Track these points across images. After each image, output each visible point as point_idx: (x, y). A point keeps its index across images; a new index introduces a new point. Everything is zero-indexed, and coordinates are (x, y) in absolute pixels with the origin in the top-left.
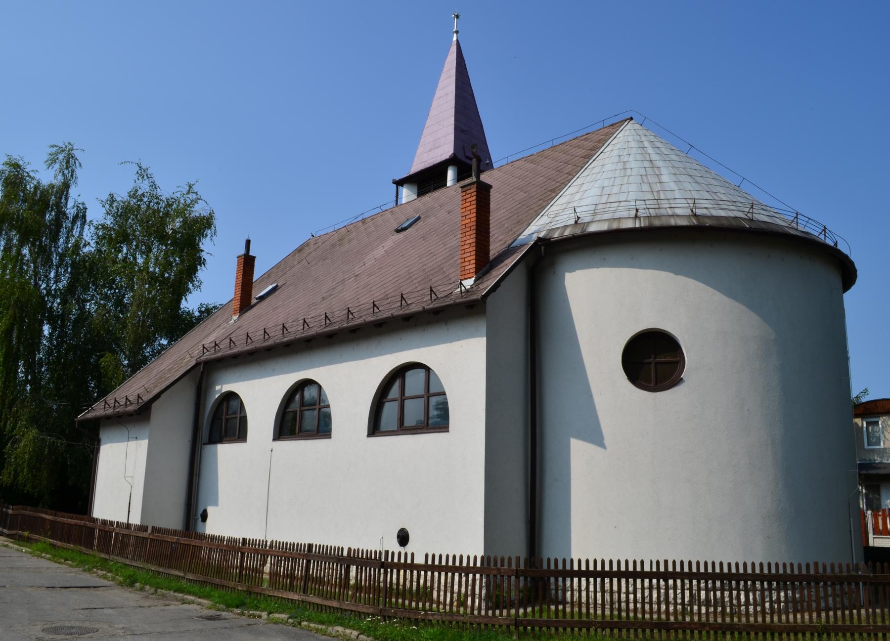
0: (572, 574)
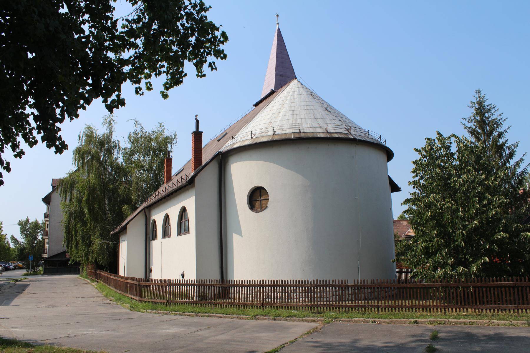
0: (234, 286)
